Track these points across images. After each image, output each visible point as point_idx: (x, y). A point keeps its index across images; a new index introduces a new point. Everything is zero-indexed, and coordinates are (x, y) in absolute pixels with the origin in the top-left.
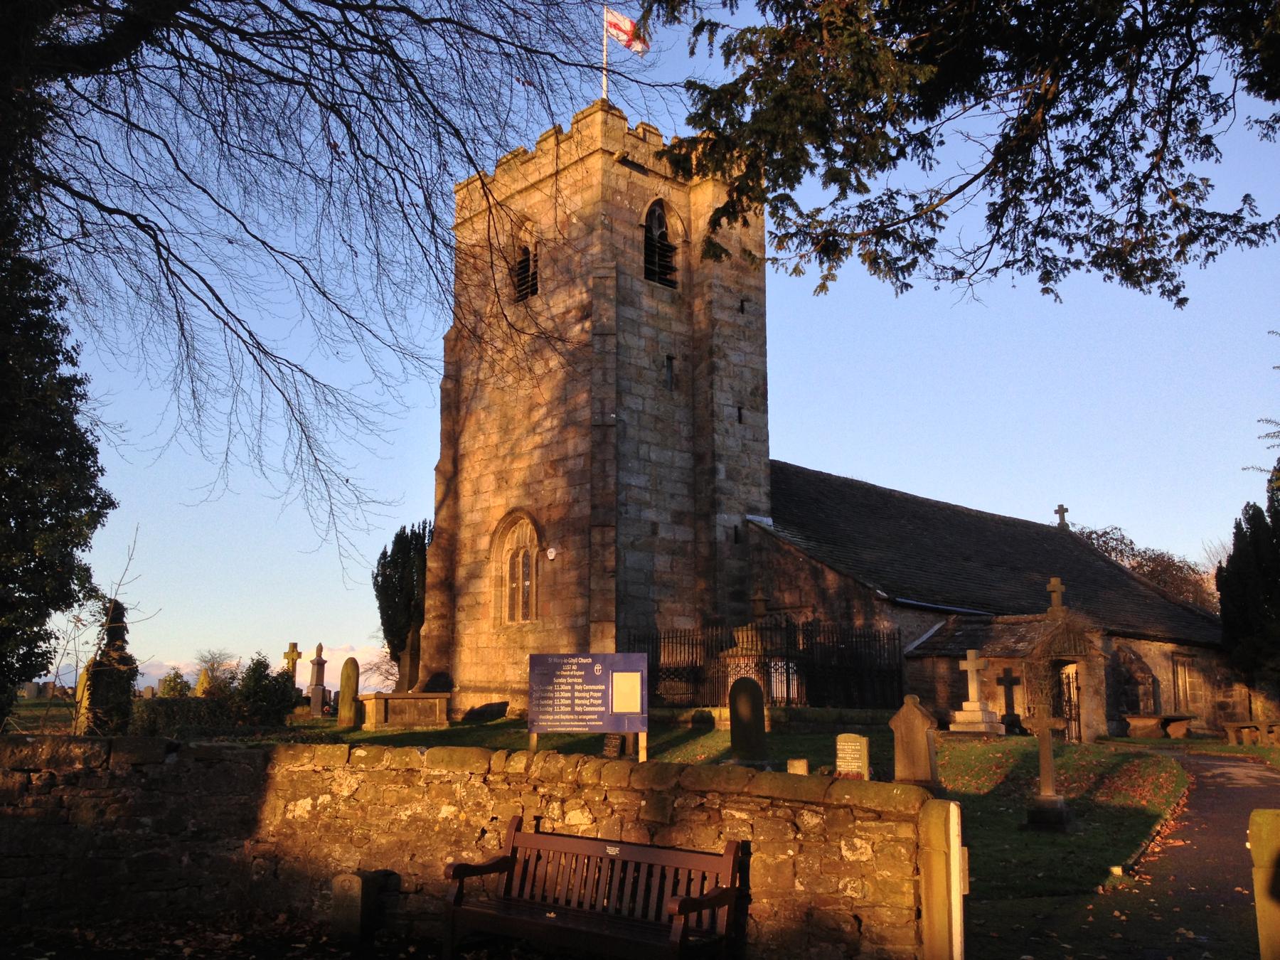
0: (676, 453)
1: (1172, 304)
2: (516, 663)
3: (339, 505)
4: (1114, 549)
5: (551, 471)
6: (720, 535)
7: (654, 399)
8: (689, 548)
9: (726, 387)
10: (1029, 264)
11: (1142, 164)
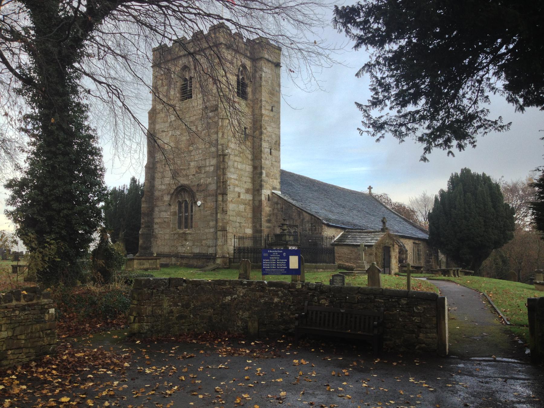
0: (247, 166)
1: (472, 146)
2: (182, 246)
6: (263, 198)
8: (251, 202)
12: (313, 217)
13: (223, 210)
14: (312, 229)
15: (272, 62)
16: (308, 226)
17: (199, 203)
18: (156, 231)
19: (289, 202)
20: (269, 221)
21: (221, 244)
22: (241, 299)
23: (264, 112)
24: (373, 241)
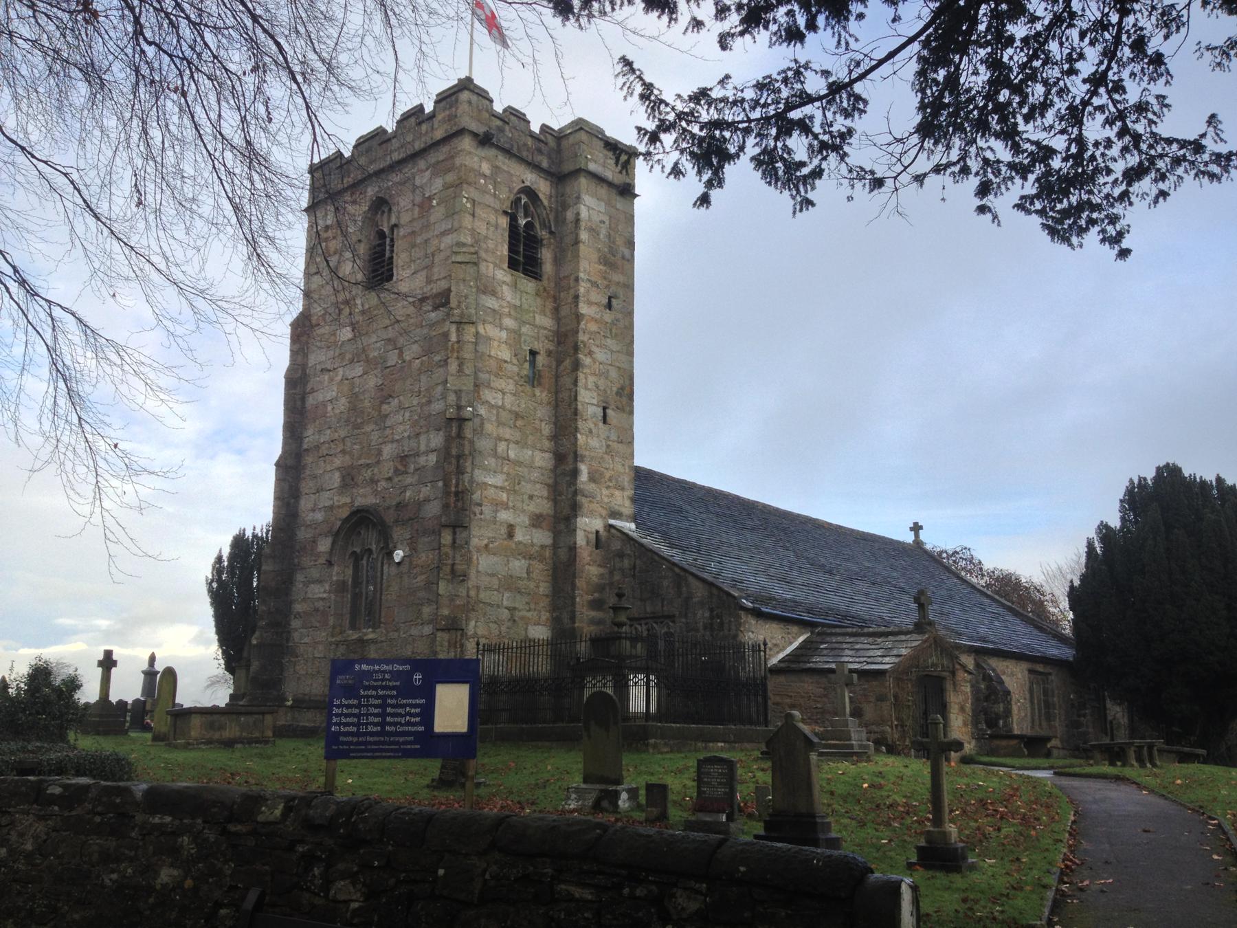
0: (537, 453)
3: (107, 476)
4: (963, 569)
5: (400, 467)
6: (580, 539)
7: (514, 395)
8: (548, 553)
9: (590, 385)
10: (965, 171)
11: (1078, 89)
12: (715, 591)
13: (453, 571)
14: (711, 624)
16: (702, 615)
17: (399, 555)
18: (296, 635)
19: (651, 550)
20: (597, 605)
22: (21, 866)
23: (584, 309)
24: (887, 659)
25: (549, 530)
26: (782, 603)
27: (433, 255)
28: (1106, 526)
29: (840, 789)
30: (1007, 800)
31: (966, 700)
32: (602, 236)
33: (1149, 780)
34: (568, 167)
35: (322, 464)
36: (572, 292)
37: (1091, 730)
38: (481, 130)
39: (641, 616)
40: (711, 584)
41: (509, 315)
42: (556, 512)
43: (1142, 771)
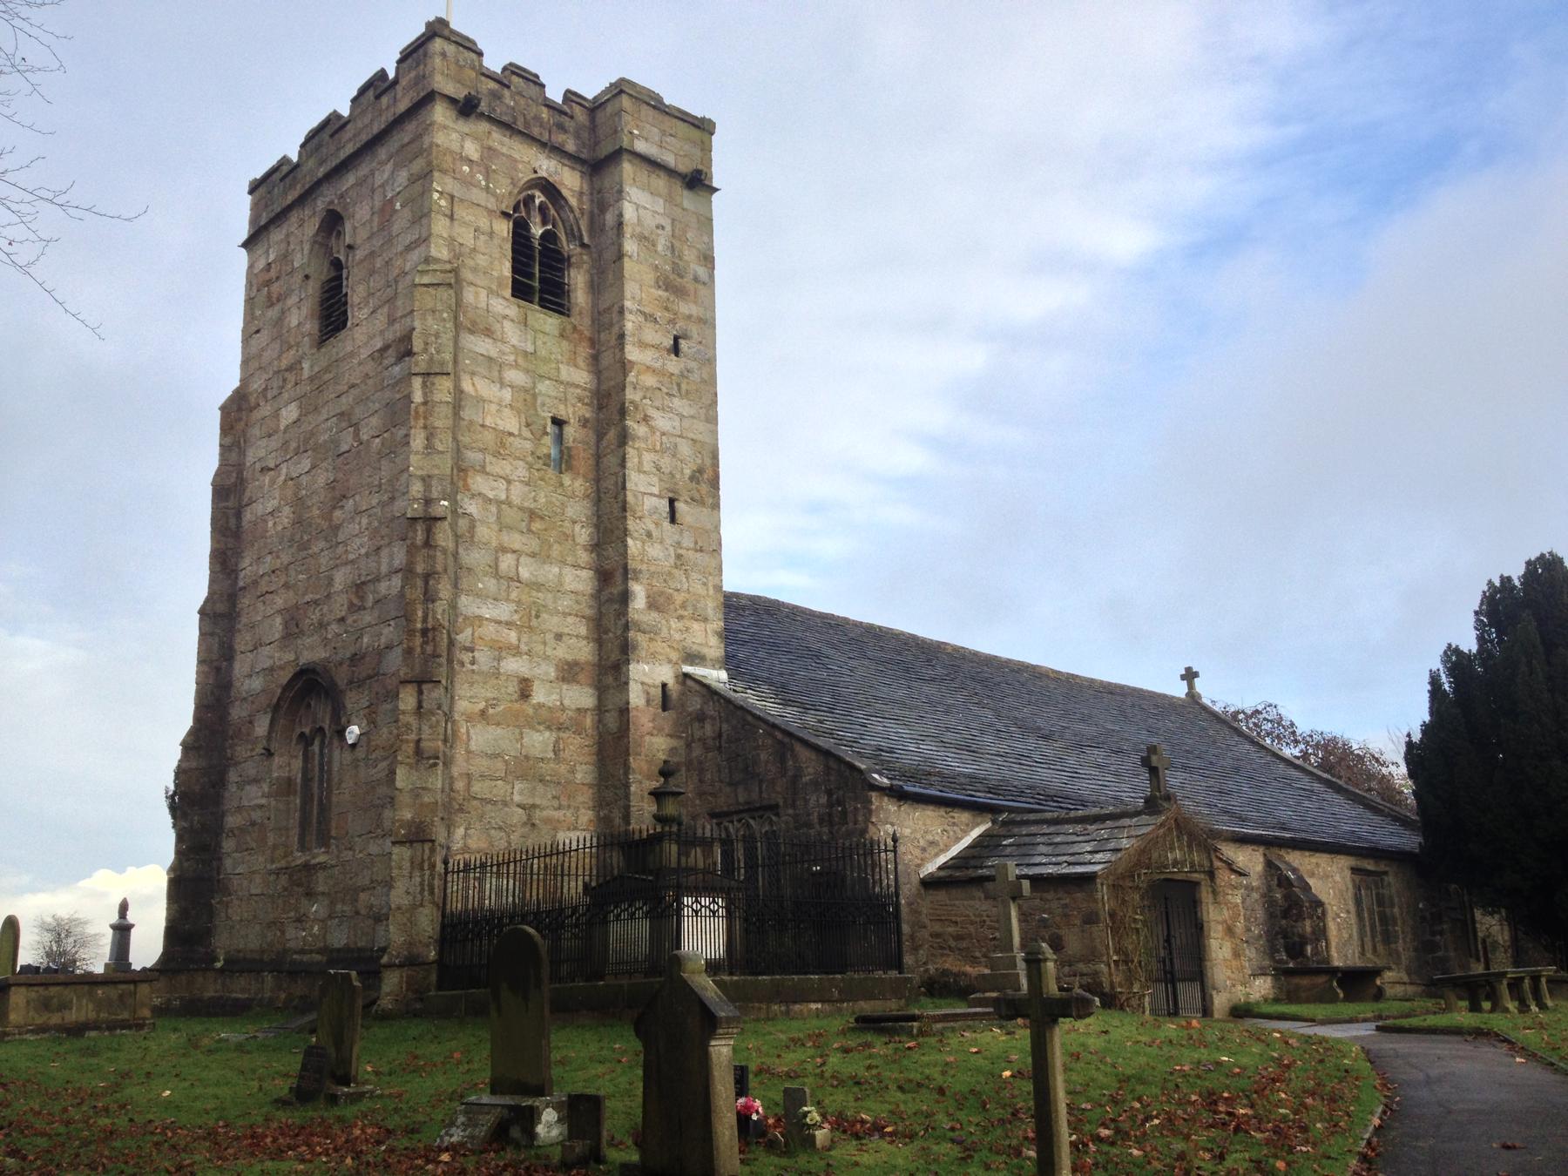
0: (568, 570)
4: (1268, 734)
5: (355, 601)
6: (636, 697)
7: (528, 484)
8: (588, 721)
12: (833, 764)
13: (418, 752)
14: (830, 815)
15: (671, 172)
16: (817, 801)
17: (353, 732)
18: (228, 863)
21: (405, 901)
23: (632, 353)
24: (1099, 857)
25: (590, 685)
26: (949, 779)
27: (396, 282)
28: (1457, 651)
29: (960, 1082)
30: (1262, 1088)
31: (1235, 918)
32: (660, 248)
33: (1530, 1037)
34: (606, 149)
35: (260, 605)
36: (615, 329)
37: (1452, 954)
38: (460, 94)
39: (732, 809)
40: (826, 754)
41: (516, 366)
42: (600, 660)
43: (1521, 1020)
